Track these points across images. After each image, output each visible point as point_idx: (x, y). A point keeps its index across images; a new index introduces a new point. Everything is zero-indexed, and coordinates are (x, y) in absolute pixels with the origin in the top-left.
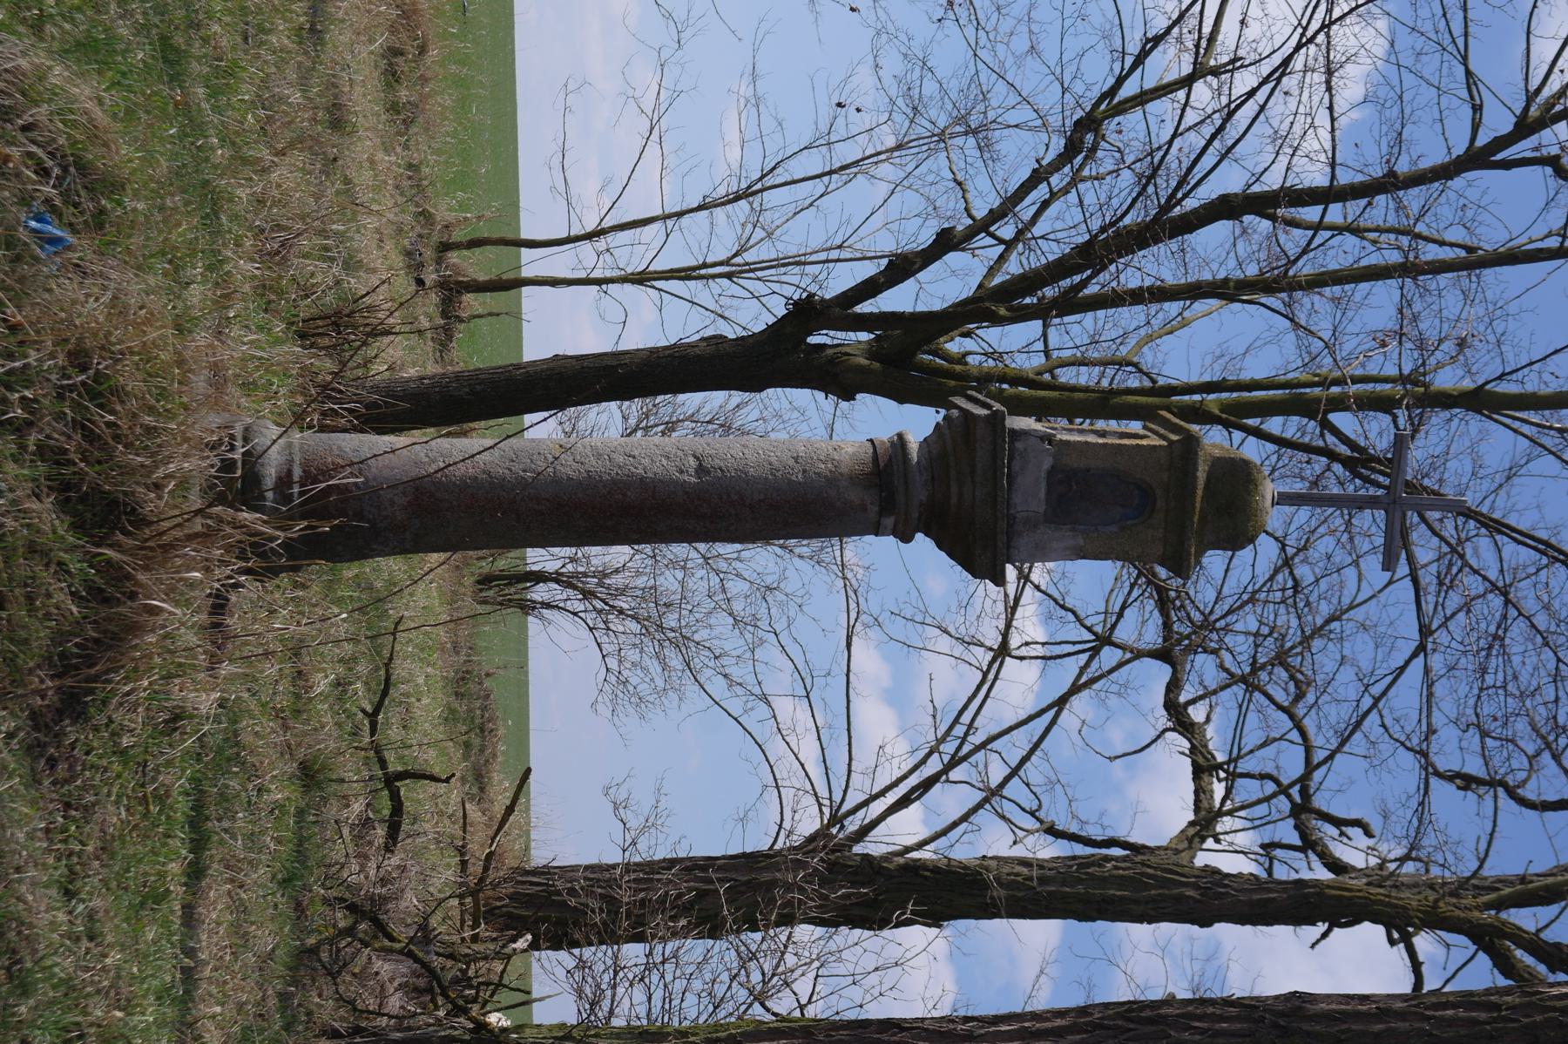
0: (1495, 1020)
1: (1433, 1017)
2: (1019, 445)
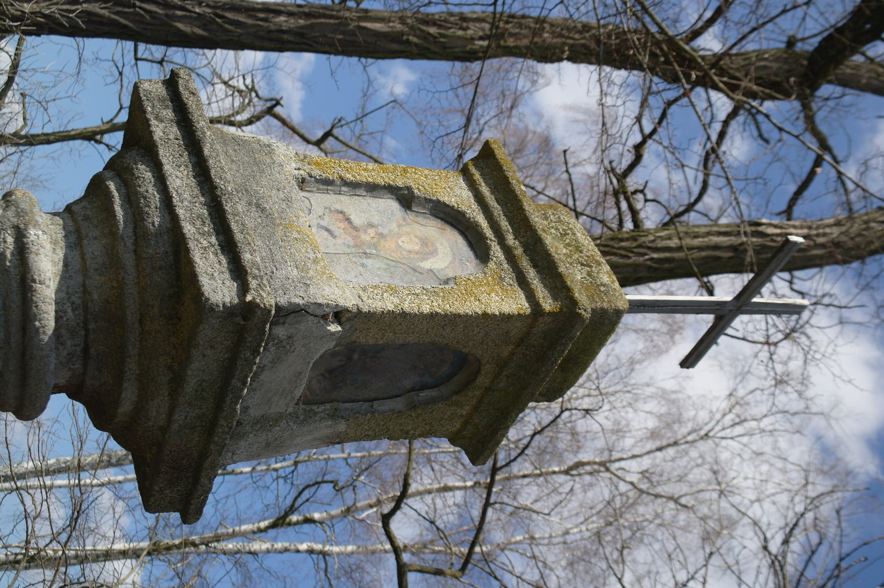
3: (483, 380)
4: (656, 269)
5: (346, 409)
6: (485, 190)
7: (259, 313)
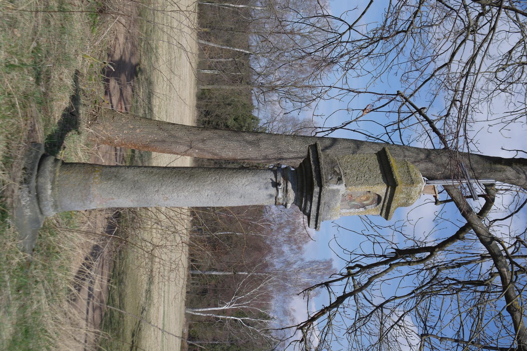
6: (389, 193)
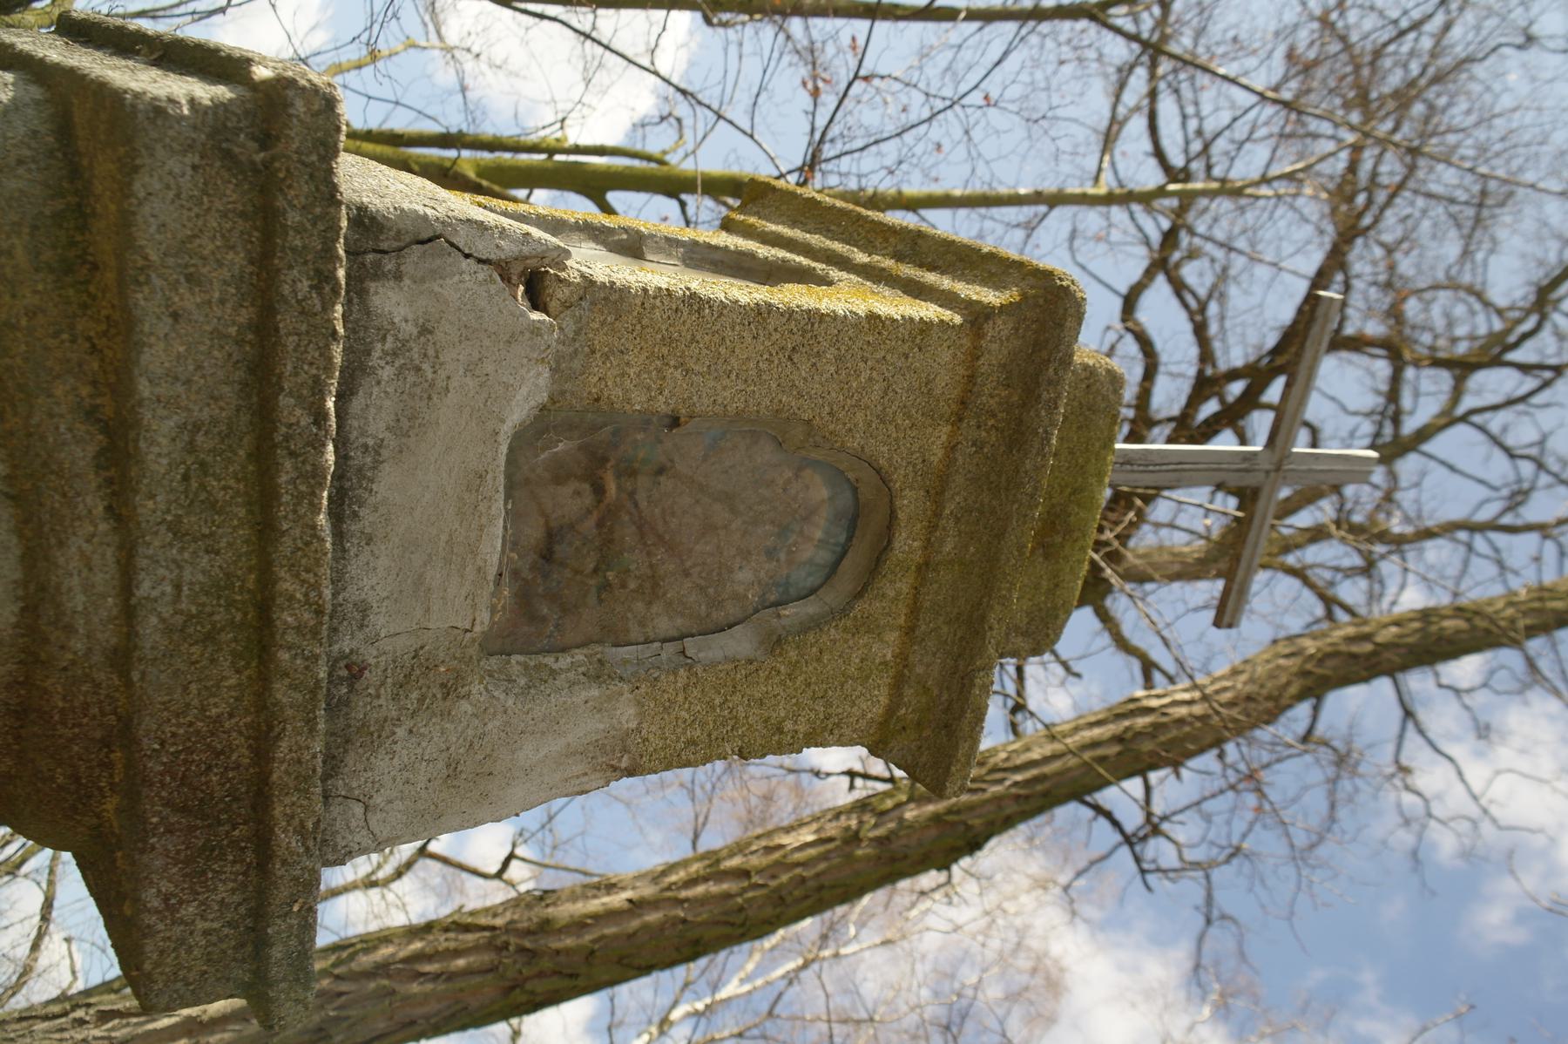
0: (744, 890)
1: (687, 900)
2: (390, 301)
3: (906, 544)
4: (1027, 797)
5: (625, 662)
7: (300, 107)
